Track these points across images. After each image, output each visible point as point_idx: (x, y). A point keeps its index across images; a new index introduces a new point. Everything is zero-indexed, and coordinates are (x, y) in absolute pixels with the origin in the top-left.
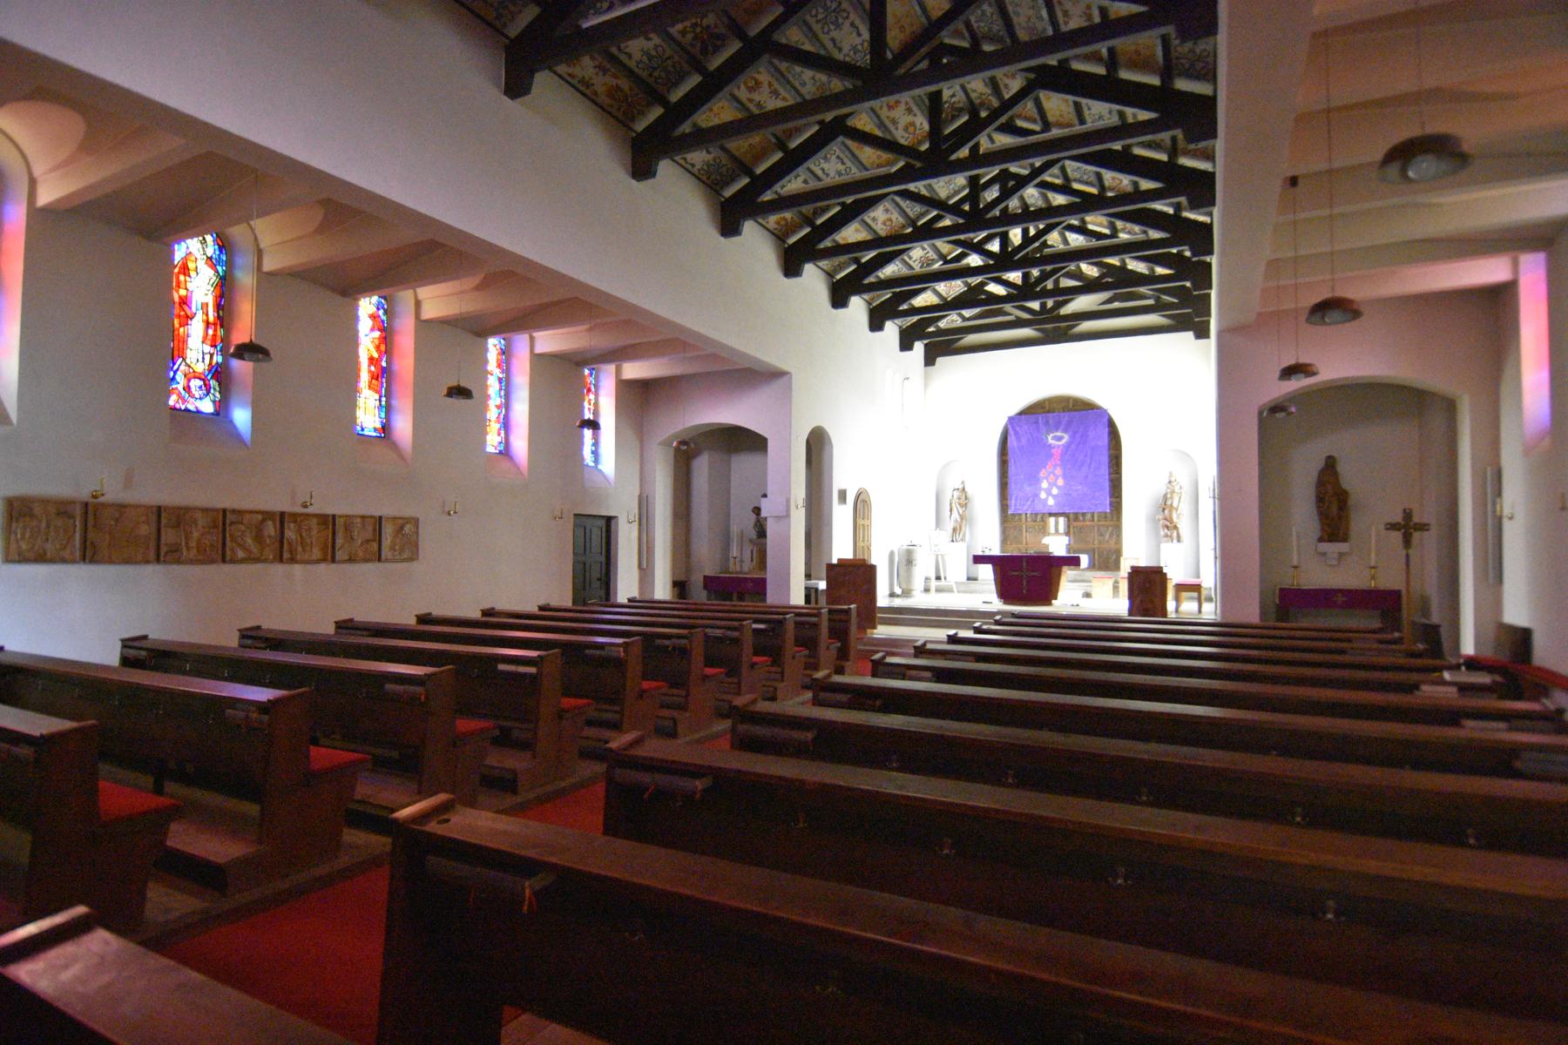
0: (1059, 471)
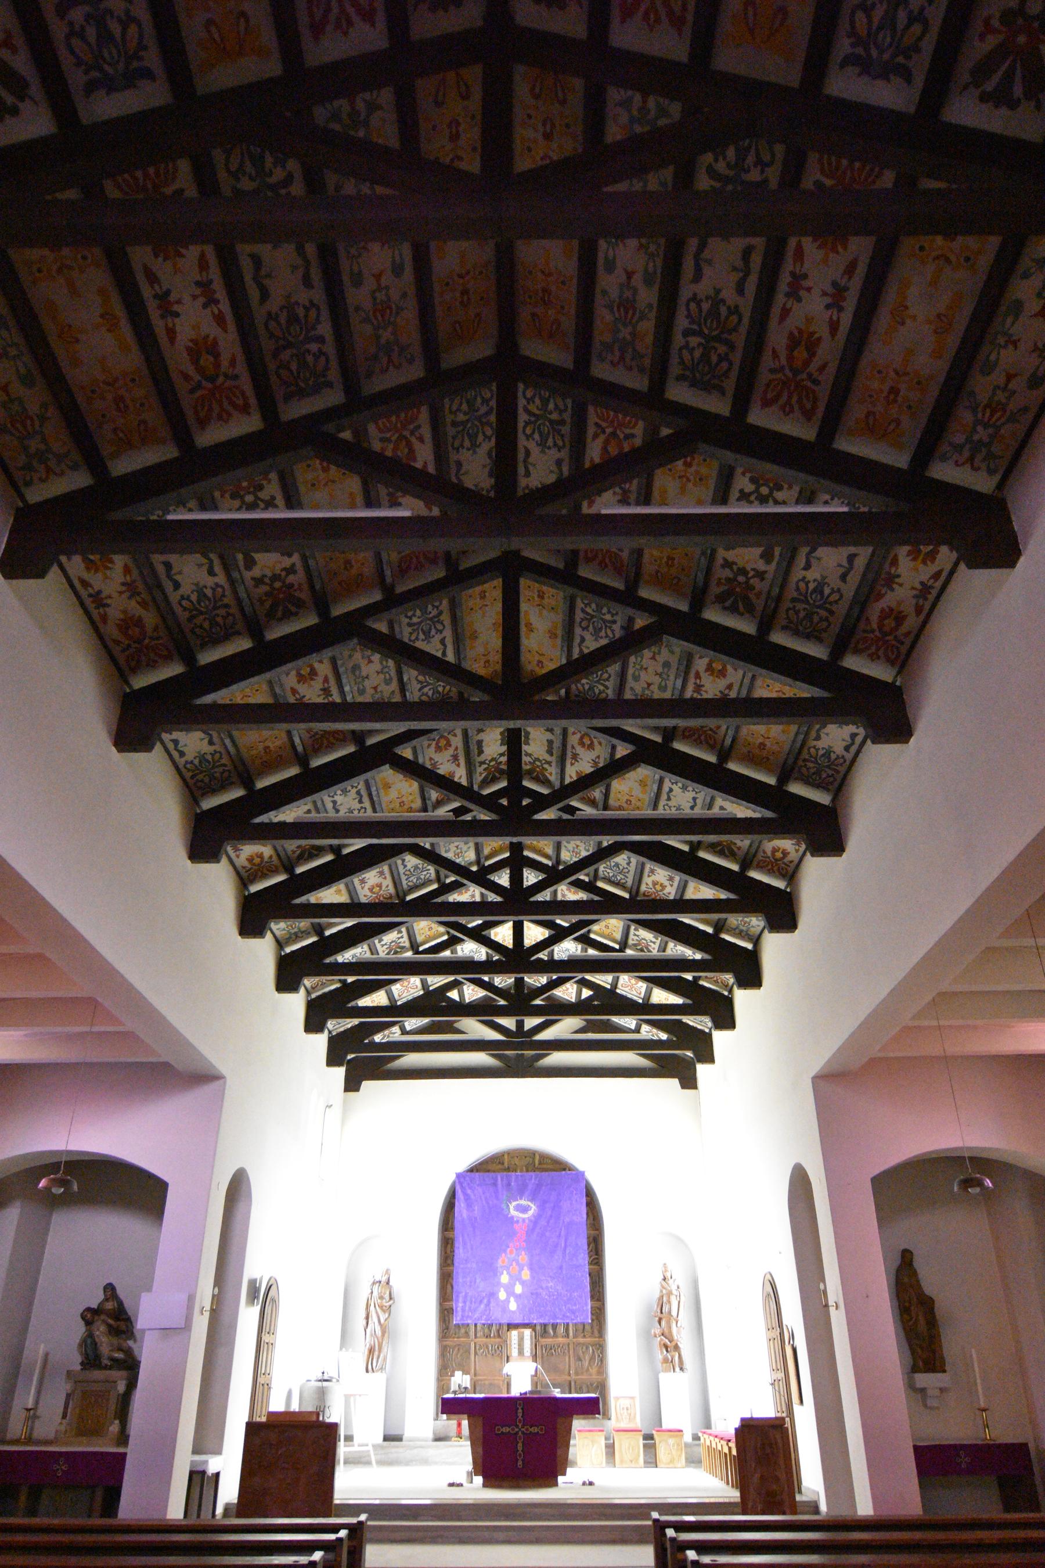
0: (524, 1258)
